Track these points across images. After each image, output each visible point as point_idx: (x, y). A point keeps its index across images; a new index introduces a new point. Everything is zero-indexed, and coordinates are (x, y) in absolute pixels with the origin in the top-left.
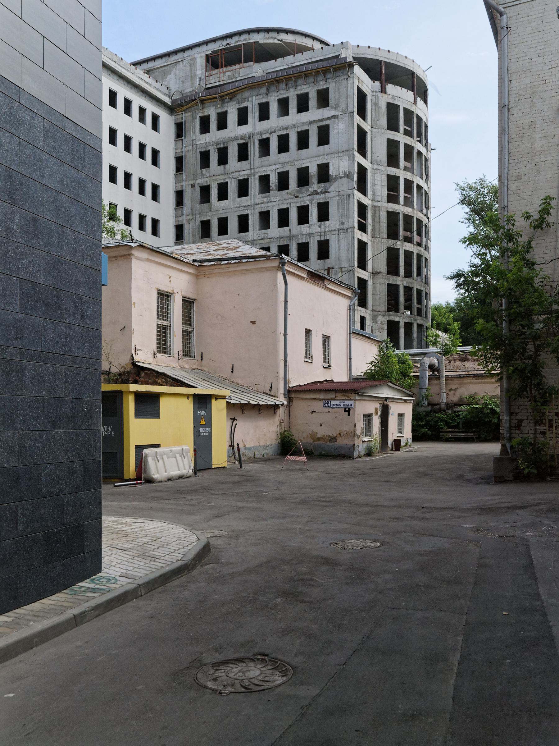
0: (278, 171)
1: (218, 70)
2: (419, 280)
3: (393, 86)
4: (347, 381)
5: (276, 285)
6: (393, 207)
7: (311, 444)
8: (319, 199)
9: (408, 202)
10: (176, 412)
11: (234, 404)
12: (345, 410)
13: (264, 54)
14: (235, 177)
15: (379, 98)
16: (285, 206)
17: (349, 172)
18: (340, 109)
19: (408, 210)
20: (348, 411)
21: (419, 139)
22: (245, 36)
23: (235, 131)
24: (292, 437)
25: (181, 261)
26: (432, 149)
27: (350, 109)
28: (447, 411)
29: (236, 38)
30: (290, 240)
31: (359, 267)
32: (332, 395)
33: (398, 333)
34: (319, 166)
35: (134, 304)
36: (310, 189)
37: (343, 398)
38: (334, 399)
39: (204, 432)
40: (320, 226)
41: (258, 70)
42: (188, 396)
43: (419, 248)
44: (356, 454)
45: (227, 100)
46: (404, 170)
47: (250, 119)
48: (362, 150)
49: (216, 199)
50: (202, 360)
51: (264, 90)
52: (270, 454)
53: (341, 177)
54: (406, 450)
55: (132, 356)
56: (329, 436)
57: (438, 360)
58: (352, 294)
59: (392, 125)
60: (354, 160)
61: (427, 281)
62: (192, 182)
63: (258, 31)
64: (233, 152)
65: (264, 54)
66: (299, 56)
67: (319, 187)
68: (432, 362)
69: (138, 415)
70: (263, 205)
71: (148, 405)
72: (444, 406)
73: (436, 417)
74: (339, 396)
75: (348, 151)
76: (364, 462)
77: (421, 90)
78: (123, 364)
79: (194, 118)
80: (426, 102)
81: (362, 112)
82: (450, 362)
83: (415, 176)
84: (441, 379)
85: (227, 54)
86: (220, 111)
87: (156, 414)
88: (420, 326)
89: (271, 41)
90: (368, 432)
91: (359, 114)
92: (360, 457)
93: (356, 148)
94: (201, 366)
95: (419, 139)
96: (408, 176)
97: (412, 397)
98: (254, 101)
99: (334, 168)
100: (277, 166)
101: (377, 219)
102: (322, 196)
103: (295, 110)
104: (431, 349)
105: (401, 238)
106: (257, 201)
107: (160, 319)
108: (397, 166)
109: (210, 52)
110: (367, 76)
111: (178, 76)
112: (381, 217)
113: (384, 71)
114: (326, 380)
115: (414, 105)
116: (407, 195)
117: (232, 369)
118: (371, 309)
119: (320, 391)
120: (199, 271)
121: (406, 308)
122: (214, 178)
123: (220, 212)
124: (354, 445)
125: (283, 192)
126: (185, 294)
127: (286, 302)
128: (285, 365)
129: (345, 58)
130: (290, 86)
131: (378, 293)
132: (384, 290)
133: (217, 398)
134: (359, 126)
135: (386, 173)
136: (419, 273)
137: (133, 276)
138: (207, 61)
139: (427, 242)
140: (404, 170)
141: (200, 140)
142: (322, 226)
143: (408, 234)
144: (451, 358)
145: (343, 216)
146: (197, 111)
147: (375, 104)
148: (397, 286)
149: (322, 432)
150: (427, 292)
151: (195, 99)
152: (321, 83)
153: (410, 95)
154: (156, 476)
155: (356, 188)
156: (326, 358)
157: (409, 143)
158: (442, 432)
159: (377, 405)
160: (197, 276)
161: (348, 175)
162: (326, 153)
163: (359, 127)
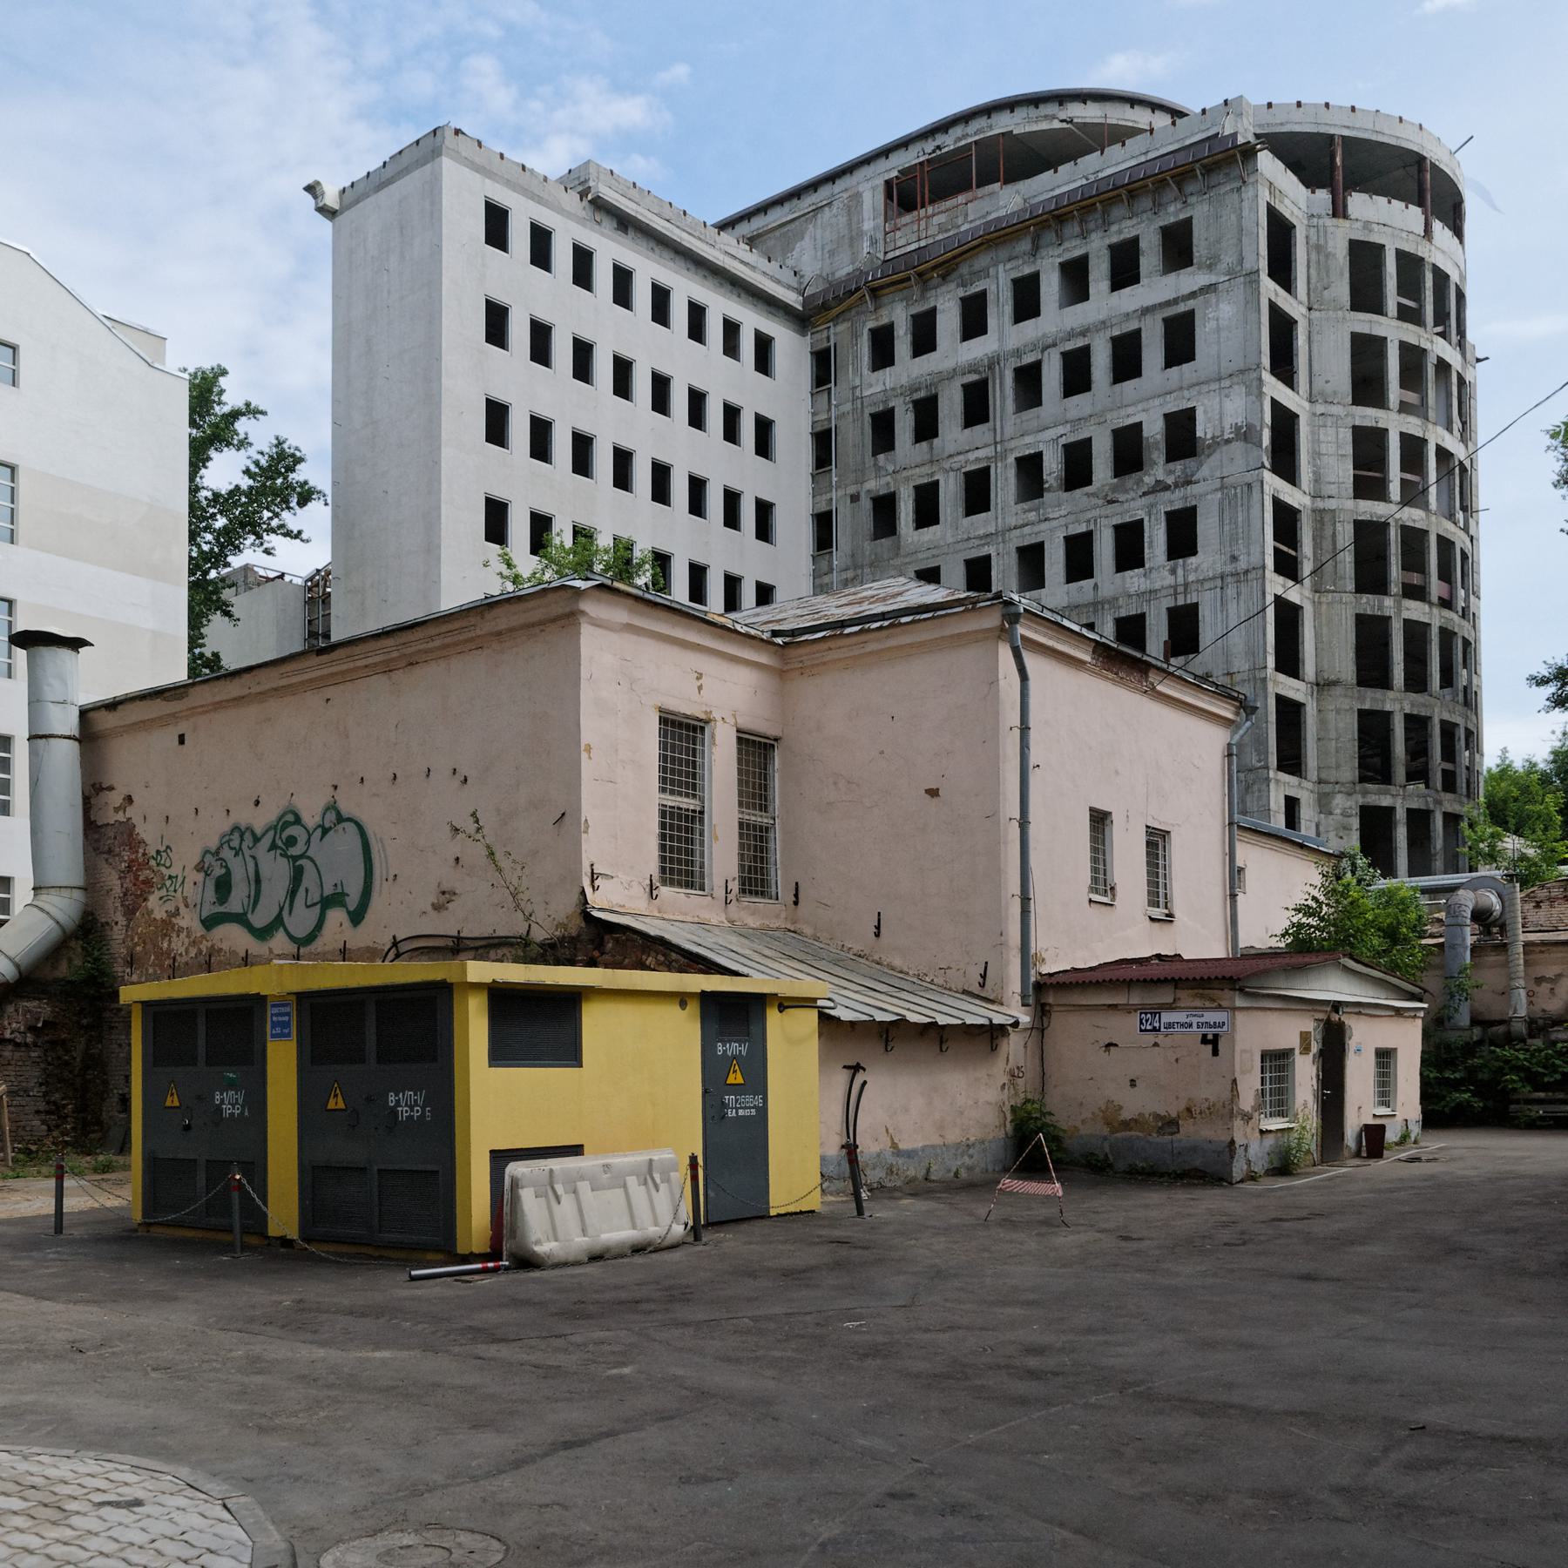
0: (1063, 441)
1: (915, 213)
2: (1448, 698)
3: (1364, 196)
4: (1222, 955)
5: (994, 682)
6: (1371, 509)
7: (1105, 1138)
8: (1171, 502)
9: (1413, 495)
10: (641, 1051)
11: (852, 1024)
12: (1204, 1040)
13: (1025, 158)
14: (956, 466)
15: (1324, 229)
16: (1082, 528)
17: (1250, 427)
18: (1222, 266)
19: (1413, 516)
20: (1212, 1042)
21: (1439, 329)
22: (981, 123)
23: (955, 353)
24: (1048, 1120)
25: (729, 629)
26: (1478, 360)
27: (1248, 266)
28: (1529, 1041)
29: (957, 131)
30: (1096, 611)
31: (1279, 668)
32: (1165, 996)
33: (1389, 840)
34: (1168, 417)
35: (589, 749)
36: (1147, 479)
37: (1198, 1003)
38: (1170, 1007)
39: (739, 1108)
40: (1173, 572)
41: (1007, 200)
42: (682, 998)
43: (1447, 613)
44: (1238, 1169)
45: (935, 281)
46: (1400, 411)
47: (992, 322)
48: (1283, 365)
49: (911, 525)
50: (796, 903)
51: (1025, 245)
52: (977, 1170)
53: (1228, 441)
54: (1403, 1155)
55: (583, 892)
56: (1157, 1117)
57: (1500, 896)
58: (1237, 714)
59: (1366, 296)
60: (1261, 394)
61: (1470, 700)
62: (852, 490)
63: (1011, 105)
64: (951, 406)
65: (1025, 158)
66: (1114, 151)
67: (1171, 472)
68: (1483, 902)
69: (500, 1055)
70: (1027, 530)
71: (539, 1027)
72: (1520, 1028)
73: (1497, 1059)
74: (1185, 997)
75: (1245, 374)
76: (1259, 1195)
77: (1443, 202)
78: (561, 917)
79: (855, 336)
80: (1458, 232)
81: (1281, 269)
82: (1538, 905)
83: (1430, 426)
84: (1511, 949)
85: (935, 170)
86: (918, 309)
87: (571, 1055)
88: (1452, 819)
89: (1044, 126)
90: (1281, 1103)
91: (1272, 275)
92: (1252, 1177)
93: (1266, 361)
94: (794, 922)
95: (1439, 329)
96: (1413, 425)
97: (1421, 1000)
98: (1001, 275)
99: (1209, 420)
100: (1061, 430)
101: (1327, 545)
102: (1179, 493)
103: (1105, 285)
104: (1484, 871)
105: (1395, 589)
106: (1012, 521)
107: (672, 792)
108: (1379, 401)
109: (895, 173)
110: (1295, 178)
111: (819, 242)
112: (1339, 538)
113: (1340, 162)
114: (1158, 956)
115: (1425, 242)
116: (1408, 476)
117: (878, 927)
118: (1315, 778)
119: (1129, 984)
120: (783, 659)
121: (1412, 776)
122: (905, 474)
123: (921, 556)
124: (1232, 1142)
125: (1078, 492)
126: (745, 723)
127: (1025, 729)
128: (1025, 912)
129: (1234, 135)
130: (1092, 225)
131: (1333, 735)
132: (1348, 727)
133: (785, 1004)
134: (1273, 306)
135: (1350, 422)
136: (1448, 679)
137: (584, 673)
138: (889, 195)
139: (1467, 599)
140: (1400, 411)
141: (871, 386)
142: (1180, 572)
143: (1415, 579)
144: (1542, 894)
145: (1234, 539)
146: (863, 317)
147: (1318, 249)
148: (1387, 715)
149: (1135, 1104)
150: (1471, 727)
151: (858, 289)
152: (1172, 209)
153: (1413, 217)
154: (545, 1247)
155: (1267, 465)
156: (1157, 891)
157: (1413, 340)
158: (1517, 1102)
159: (1308, 1024)
160: (781, 674)
161: (1246, 434)
162: (1185, 384)
163: (1274, 309)
